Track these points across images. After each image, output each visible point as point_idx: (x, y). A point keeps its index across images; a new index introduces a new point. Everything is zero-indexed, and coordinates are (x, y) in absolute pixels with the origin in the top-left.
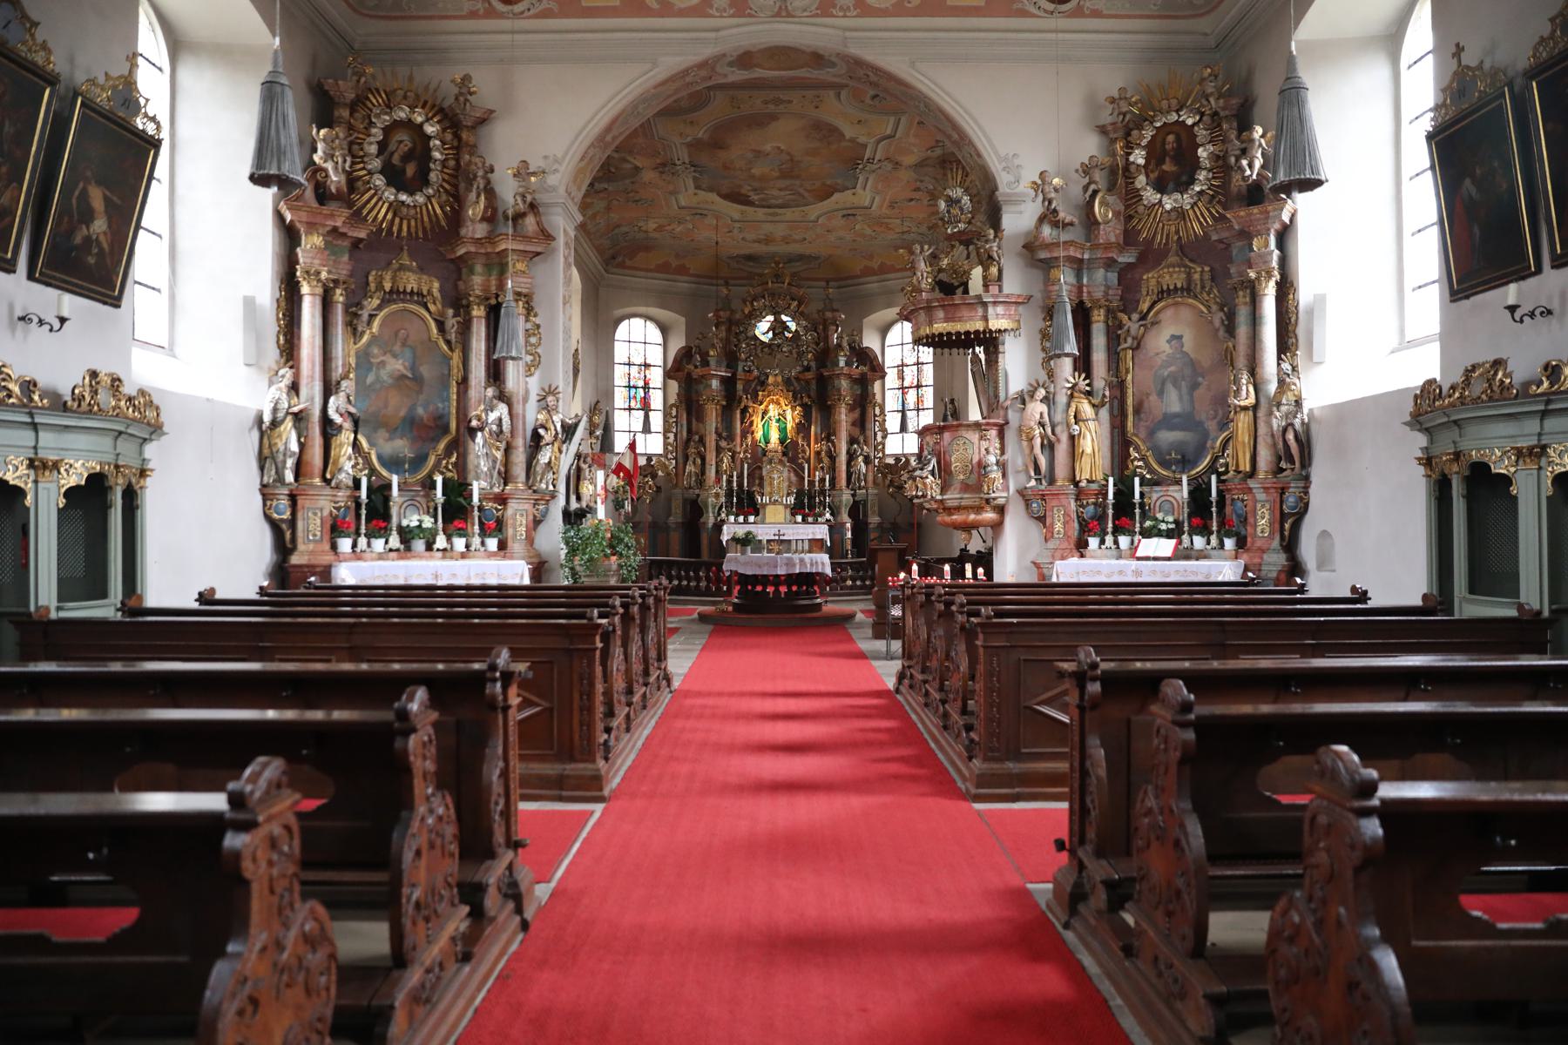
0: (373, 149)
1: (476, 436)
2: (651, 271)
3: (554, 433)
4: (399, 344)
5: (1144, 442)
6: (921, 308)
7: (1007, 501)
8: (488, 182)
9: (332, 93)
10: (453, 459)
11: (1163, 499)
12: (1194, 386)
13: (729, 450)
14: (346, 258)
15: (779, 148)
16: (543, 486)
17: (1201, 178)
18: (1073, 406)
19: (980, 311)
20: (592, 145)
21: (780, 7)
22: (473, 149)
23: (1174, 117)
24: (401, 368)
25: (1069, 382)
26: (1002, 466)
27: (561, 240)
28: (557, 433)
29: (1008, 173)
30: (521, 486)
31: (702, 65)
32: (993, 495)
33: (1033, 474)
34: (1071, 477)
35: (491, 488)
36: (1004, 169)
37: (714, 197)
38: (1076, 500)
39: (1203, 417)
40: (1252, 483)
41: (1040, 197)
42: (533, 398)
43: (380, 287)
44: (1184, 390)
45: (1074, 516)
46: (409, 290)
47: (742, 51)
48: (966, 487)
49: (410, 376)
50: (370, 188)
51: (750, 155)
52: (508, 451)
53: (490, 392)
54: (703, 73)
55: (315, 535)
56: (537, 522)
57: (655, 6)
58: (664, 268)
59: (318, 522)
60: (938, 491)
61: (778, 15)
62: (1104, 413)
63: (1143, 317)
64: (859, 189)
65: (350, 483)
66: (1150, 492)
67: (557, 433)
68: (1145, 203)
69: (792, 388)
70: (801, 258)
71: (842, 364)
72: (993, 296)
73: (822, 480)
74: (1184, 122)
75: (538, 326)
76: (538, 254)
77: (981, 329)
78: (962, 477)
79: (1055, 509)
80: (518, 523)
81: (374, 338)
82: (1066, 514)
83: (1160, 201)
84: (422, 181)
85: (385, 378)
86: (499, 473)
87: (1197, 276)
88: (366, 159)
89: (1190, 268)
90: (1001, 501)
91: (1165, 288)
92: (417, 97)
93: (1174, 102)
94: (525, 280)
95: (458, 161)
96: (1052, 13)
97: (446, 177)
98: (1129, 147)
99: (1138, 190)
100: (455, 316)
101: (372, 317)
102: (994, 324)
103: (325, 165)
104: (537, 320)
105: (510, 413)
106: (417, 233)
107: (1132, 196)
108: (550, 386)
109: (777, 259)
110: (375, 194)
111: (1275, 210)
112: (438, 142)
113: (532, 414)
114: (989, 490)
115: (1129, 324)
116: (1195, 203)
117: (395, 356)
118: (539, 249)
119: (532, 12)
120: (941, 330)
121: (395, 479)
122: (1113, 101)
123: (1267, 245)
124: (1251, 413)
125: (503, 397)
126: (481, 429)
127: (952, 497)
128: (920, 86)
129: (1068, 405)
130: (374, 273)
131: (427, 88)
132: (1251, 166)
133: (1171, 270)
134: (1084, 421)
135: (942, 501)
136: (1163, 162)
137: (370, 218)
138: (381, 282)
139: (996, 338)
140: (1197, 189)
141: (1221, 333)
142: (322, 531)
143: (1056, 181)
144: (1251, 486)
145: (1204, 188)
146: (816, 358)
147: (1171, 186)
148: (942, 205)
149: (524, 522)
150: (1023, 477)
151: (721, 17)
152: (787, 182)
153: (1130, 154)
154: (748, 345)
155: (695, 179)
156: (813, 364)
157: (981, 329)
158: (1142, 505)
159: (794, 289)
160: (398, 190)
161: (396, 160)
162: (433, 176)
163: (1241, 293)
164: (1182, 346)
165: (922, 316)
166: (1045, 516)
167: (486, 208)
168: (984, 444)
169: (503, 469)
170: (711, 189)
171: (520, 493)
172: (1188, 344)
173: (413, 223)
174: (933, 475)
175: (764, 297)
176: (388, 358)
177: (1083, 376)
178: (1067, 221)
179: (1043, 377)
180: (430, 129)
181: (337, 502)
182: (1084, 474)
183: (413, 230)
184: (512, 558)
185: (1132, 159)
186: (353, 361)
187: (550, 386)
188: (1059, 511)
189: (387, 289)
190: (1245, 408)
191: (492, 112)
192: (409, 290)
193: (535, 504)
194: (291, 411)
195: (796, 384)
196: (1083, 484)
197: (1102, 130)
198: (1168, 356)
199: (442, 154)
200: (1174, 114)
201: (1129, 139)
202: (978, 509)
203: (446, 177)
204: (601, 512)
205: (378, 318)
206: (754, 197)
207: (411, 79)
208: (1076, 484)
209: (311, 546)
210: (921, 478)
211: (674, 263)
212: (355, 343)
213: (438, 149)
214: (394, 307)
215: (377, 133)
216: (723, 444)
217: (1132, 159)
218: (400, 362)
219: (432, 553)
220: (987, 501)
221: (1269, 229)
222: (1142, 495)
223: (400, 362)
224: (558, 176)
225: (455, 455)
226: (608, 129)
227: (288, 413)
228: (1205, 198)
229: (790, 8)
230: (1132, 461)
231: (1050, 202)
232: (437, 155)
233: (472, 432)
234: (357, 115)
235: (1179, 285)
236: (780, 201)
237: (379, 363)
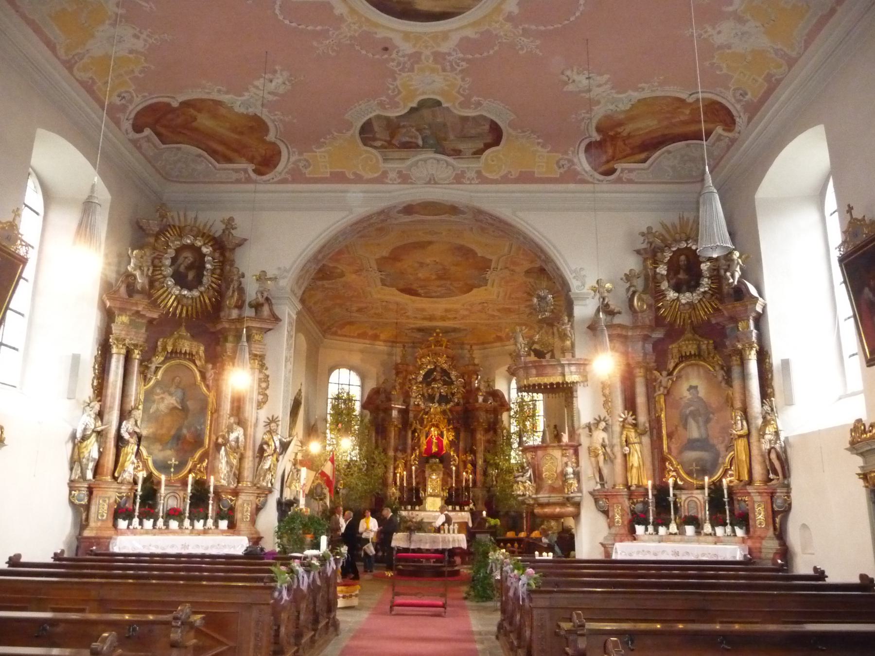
0: (168, 262)
1: (221, 449)
2: (353, 337)
3: (273, 448)
5: (676, 458)
6: (521, 368)
7: (581, 499)
8: (240, 283)
9: (145, 228)
10: (205, 464)
11: (689, 499)
12: (707, 421)
13: (403, 459)
14: (143, 330)
15: (435, 261)
16: (264, 484)
17: (704, 283)
18: (625, 433)
19: (560, 369)
20: (309, 261)
21: (430, 179)
22: (232, 263)
23: (683, 245)
24: (174, 402)
25: (621, 417)
26: (577, 475)
27: (286, 320)
28: (276, 448)
29: (577, 280)
30: (249, 484)
31: (382, 212)
32: (572, 495)
33: (598, 480)
34: (625, 483)
36: (574, 278)
37: (394, 291)
38: (629, 499)
39: (715, 442)
40: (750, 489)
41: (598, 295)
42: (261, 424)
43: (164, 349)
44: (701, 423)
45: (629, 511)
46: (183, 351)
47: (405, 205)
48: (553, 489)
50: (164, 286)
51: (416, 265)
52: (241, 459)
53: (232, 420)
54: (382, 217)
55: (103, 516)
56: (258, 509)
57: (352, 177)
58: (362, 336)
59: (106, 507)
60: (534, 491)
61: (429, 182)
62: (646, 440)
63: (670, 374)
64: (489, 286)
65: (131, 480)
66: (680, 494)
67: (276, 448)
68: (668, 298)
69: (447, 417)
70: (455, 330)
71: (481, 399)
72: (568, 360)
73: (467, 481)
74: (690, 247)
76: (270, 330)
77: (561, 382)
78: (550, 482)
79: (615, 506)
80: (245, 509)
81: (158, 383)
82: (622, 509)
83: (678, 298)
84: (198, 281)
86: (235, 474)
87: (704, 347)
88: (163, 268)
89: (700, 341)
90: (577, 499)
91: (684, 354)
92: (199, 231)
93: (683, 235)
94: (260, 346)
95: (222, 270)
96: (602, 181)
97: (214, 280)
98: (656, 263)
99: (663, 291)
101: (157, 369)
102: (569, 378)
103: (135, 272)
104: (267, 372)
105: (245, 435)
106: (192, 314)
107: (659, 295)
109: (438, 330)
110: (167, 290)
111: (751, 304)
112: (210, 258)
113: (260, 434)
114: (568, 491)
115: (661, 378)
116: (701, 299)
117: (171, 394)
118: (270, 327)
119: (275, 180)
120: (534, 382)
121: (163, 478)
122: (643, 234)
123: (748, 327)
124: (745, 440)
125: (241, 423)
126: (225, 445)
127: (543, 497)
128: (519, 226)
129: (621, 434)
130: (161, 340)
131: (205, 225)
132: (733, 276)
133: (687, 342)
134: (632, 444)
135: (535, 499)
136: (678, 273)
137: (162, 305)
138: (165, 346)
139: (571, 388)
140: (702, 290)
141: (723, 384)
142: (107, 514)
143: (608, 286)
144: (750, 491)
145: (707, 289)
146: (463, 398)
147: (684, 288)
148: (535, 300)
149: (249, 509)
150: (593, 483)
151: (393, 184)
152: (443, 282)
153: (656, 268)
154: (418, 387)
155: (382, 280)
156: (461, 401)
157: (561, 382)
158: (675, 503)
159: (450, 351)
160: (182, 288)
161: (182, 269)
162: (205, 280)
163: (734, 358)
164: (698, 393)
165: (521, 372)
166: (608, 511)
167: (238, 300)
168: (565, 459)
169: (237, 472)
170: (392, 286)
172: (702, 392)
173: (190, 308)
174: (530, 480)
175: (429, 356)
176: (166, 396)
177: (631, 413)
178: (615, 311)
179: (603, 414)
180: (205, 250)
182: (634, 482)
183: (190, 313)
184: (239, 534)
185: (658, 270)
186: (142, 397)
187: (273, 416)
188: (618, 507)
189: (169, 351)
190: (740, 436)
191: (245, 240)
192: (183, 351)
193: (257, 497)
194: (96, 430)
195: (449, 414)
196: (633, 488)
197: (638, 252)
198: (689, 399)
199: (212, 265)
200: (684, 242)
201: (656, 258)
202: (562, 504)
203: (214, 280)
204: (302, 501)
205: (162, 369)
206: (421, 291)
207: (196, 219)
208: (628, 487)
209: (99, 524)
210: (522, 482)
211: (371, 333)
212: (145, 386)
213: (209, 263)
215: (171, 252)
216: (399, 455)
217: (658, 270)
218: (174, 398)
220: (568, 499)
221: (749, 317)
222: (674, 495)
223: (174, 398)
224: (286, 280)
225: (206, 461)
226: (320, 251)
227: (93, 431)
228: (708, 296)
229: (436, 179)
230: (668, 472)
231: (604, 299)
232: (208, 266)
233: (218, 447)
234: (159, 241)
235: (693, 353)
236: (438, 294)
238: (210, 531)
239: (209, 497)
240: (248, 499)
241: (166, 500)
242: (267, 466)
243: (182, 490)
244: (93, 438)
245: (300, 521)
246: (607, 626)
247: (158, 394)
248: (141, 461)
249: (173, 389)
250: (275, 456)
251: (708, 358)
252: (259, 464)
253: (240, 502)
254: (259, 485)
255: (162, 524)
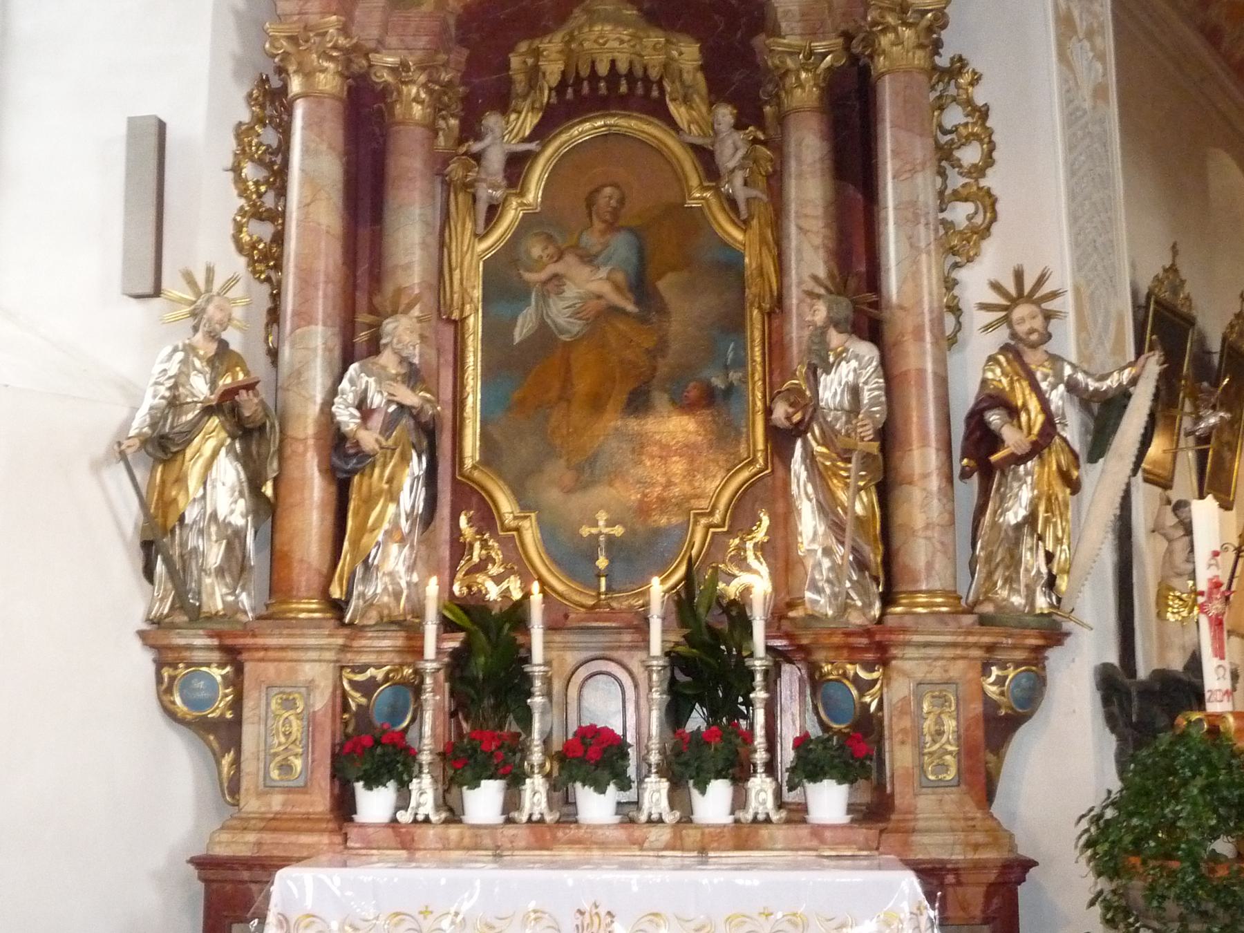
3: (1039, 420)
4: (598, 225)
10: (760, 535)
24: (606, 289)
35: (845, 608)
49: (631, 307)
55: (286, 767)
59: (296, 727)
75: (983, 114)
80: (928, 725)
81: (529, 223)
85: (561, 321)
100: (739, 126)
101: (517, 165)
105: (886, 366)
108: (1019, 276)
117: (588, 259)
126: (800, 430)
149: (950, 725)
171: (932, 624)
176: (570, 266)
181: (363, 669)
187: (1019, 276)
214: (584, 130)
218: (603, 273)
219: (638, 833)
223: (603, 273)
225: (766, 521)
237: (545, 283)
238: (764, 832)
239: (751, 675)
240: (936, 675)
241: (573, 692)
242: (1015, 514)
243: (633, 648)
244: (213, 436)
245: (1208, 788)
246: (475, 356)
247: (538, 265)
248: (494, 535)
249: (591, 240)
250: (1055, 459)
251: (1162, 867)
252: (981, 510)
253: (899, 689)
254: (988, 608)
255: (542, 798)
